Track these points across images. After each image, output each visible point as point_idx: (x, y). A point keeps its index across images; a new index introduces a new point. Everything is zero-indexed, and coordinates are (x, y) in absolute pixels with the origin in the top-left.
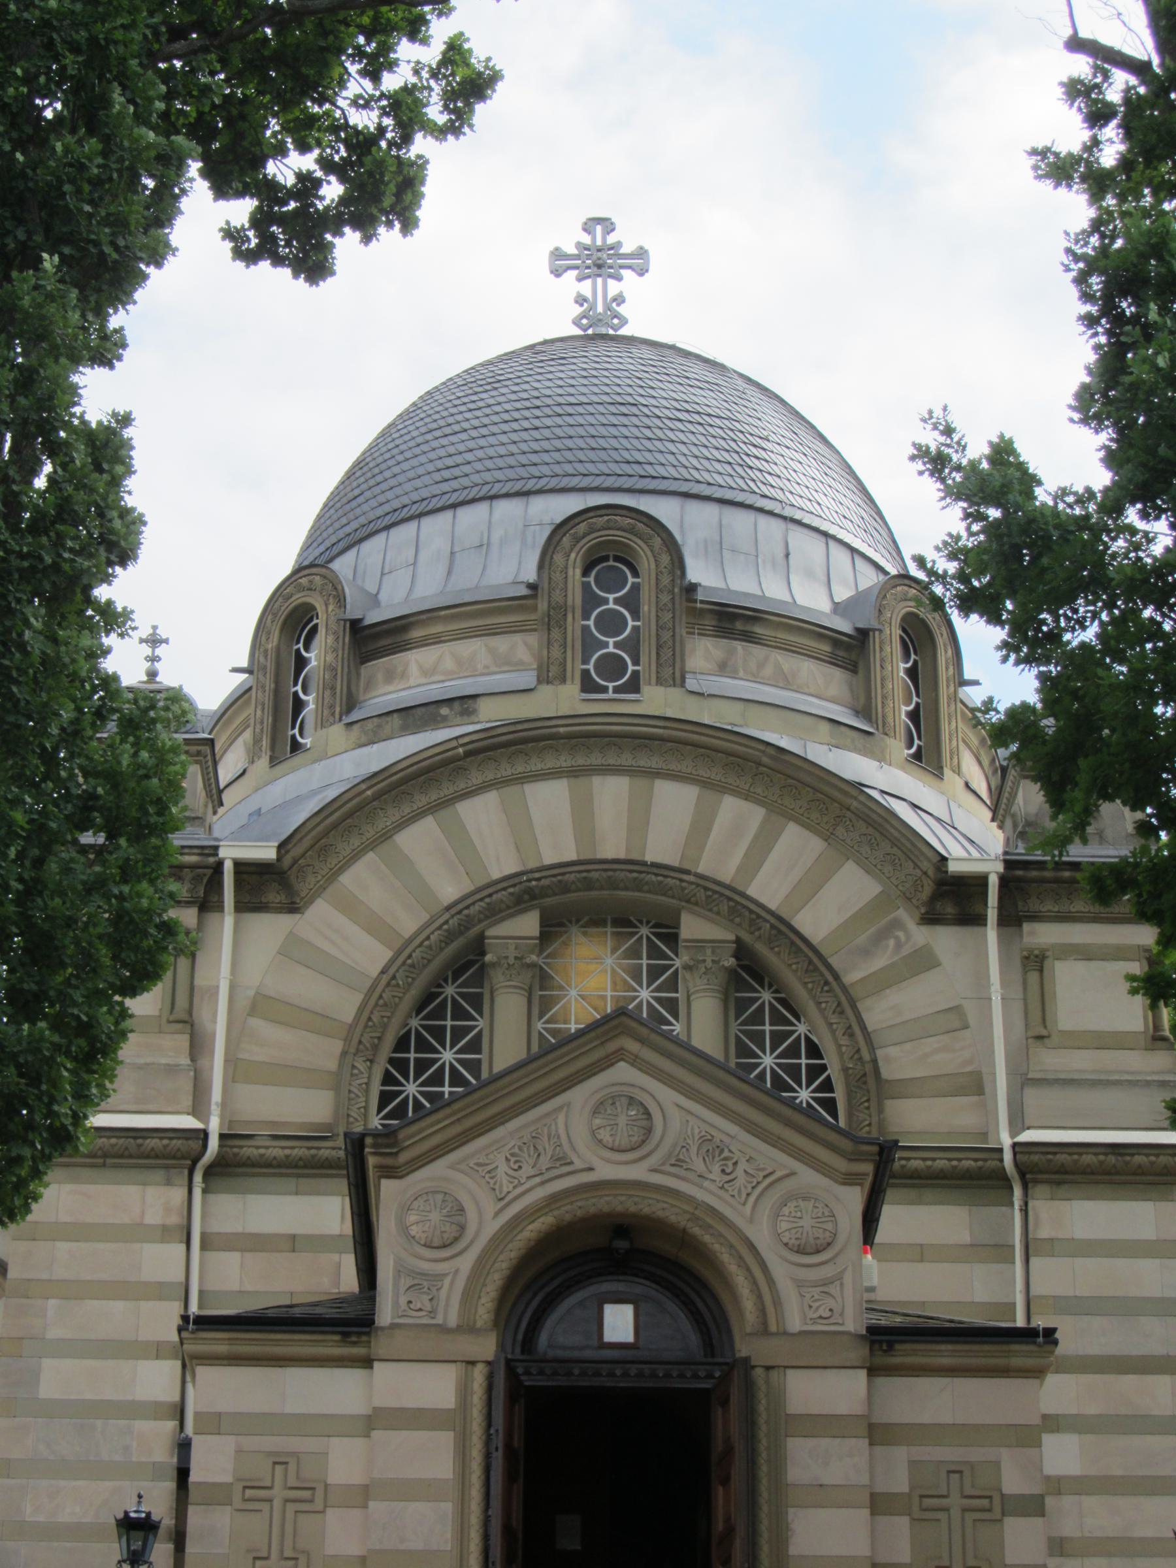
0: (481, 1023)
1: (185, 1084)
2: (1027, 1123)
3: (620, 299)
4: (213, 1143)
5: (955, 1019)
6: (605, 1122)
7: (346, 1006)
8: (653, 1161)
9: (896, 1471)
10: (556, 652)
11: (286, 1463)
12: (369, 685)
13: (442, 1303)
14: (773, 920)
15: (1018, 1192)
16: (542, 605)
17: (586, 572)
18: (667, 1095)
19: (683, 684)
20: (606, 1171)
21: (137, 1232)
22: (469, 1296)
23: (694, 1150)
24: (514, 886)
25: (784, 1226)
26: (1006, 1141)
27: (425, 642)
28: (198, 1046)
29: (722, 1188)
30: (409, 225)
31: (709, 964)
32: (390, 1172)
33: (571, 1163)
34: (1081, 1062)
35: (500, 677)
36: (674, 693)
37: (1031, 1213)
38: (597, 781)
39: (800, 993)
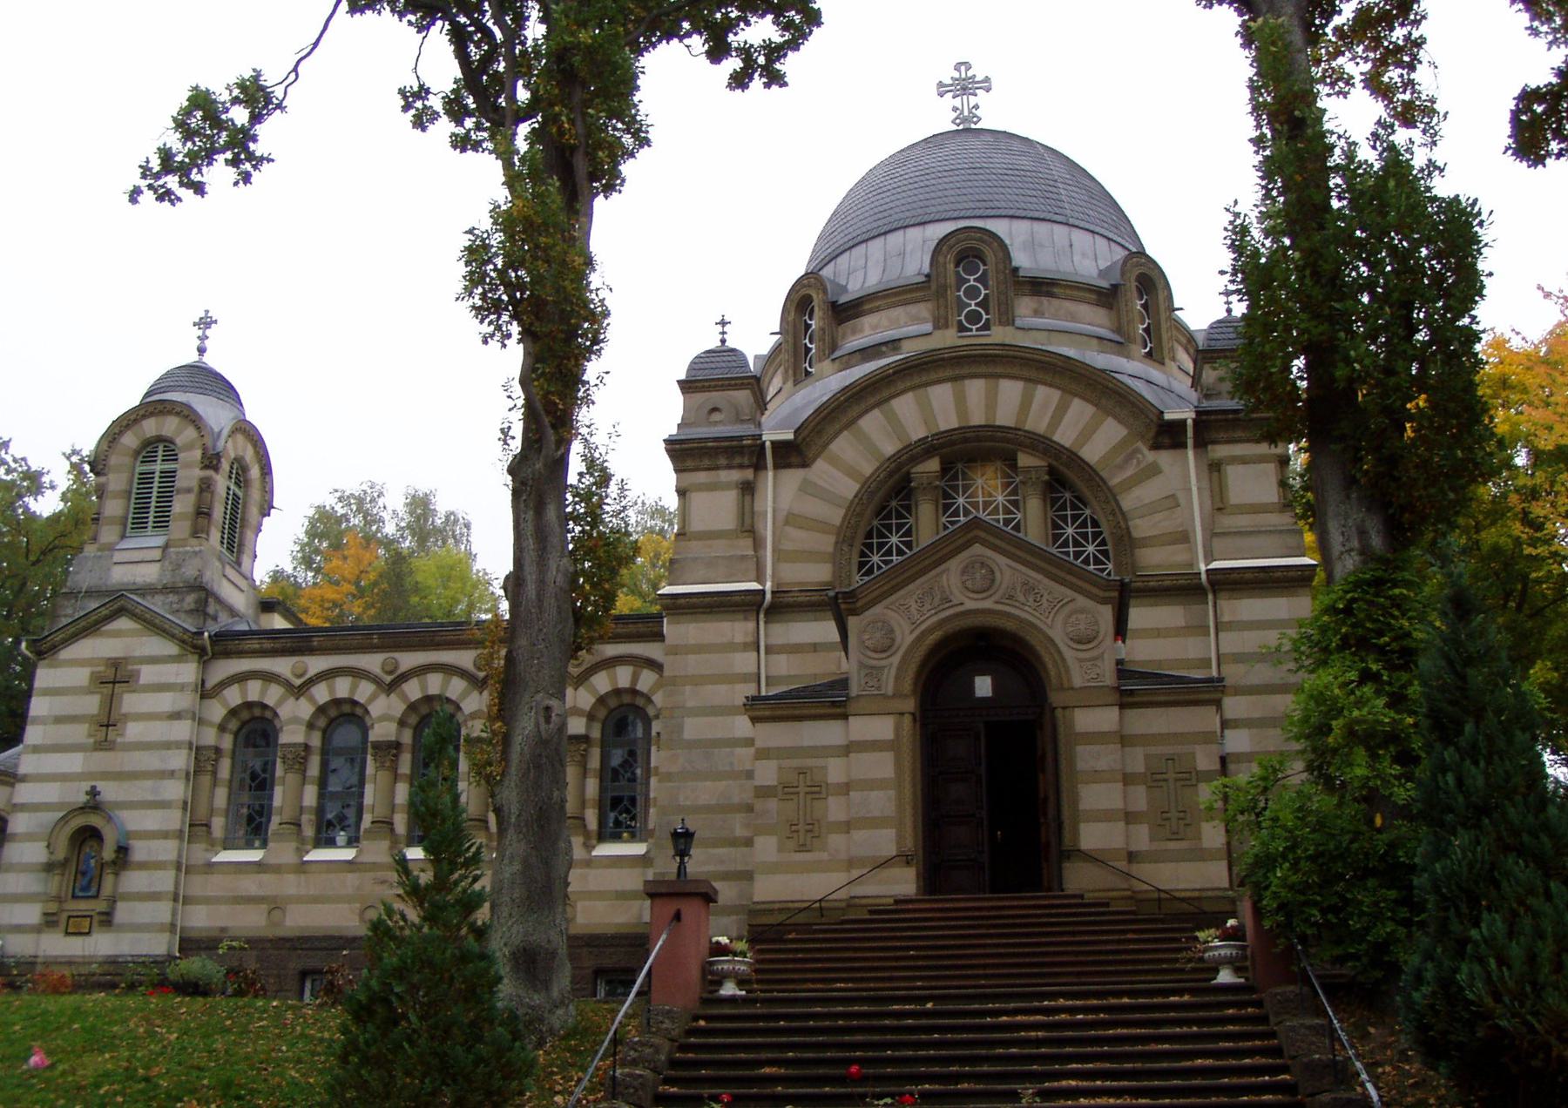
0: (911, 520)
1: (752, 565)
3: (976, 107)
4: (768, 596)
5: (1171, 502)
7: (836, 516)
8: (996, 597)
9: (1137, 761)
10: (942, 312)
12: (843, 337)
15: (1210, 597)
16: (934, 286)
17: (957, 265)
18: (1002, 560)
20: (970, 605)
21: (731, 647)
26: (1203, 568)
27: (871, 311)
28: (758, 544)
30: (679, 382)
34: (1243, 521)
35: (912, 329)
36: (1009, 329)
38: (967, 382)
39: (1087, 493)
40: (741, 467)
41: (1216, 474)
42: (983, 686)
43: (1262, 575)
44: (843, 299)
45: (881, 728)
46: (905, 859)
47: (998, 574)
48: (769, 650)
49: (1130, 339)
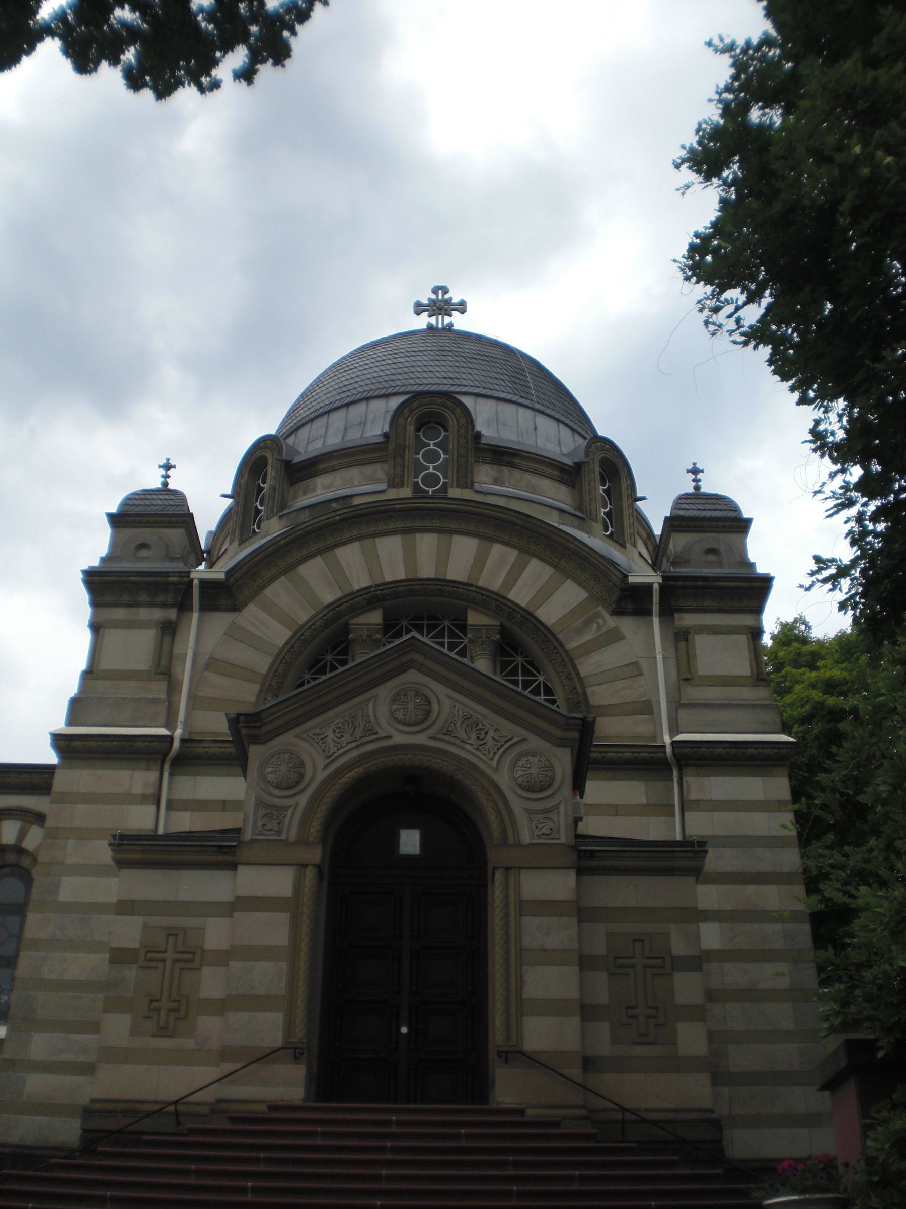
1: (162, 709)
2: (680, 730)
4: (176, 744)
5: (634, 670)
6: (399, 707)
8: (432, 732)
11: (177, 935)
13: (286, 827)
14: (523, 612)
15: (675, 773)
16: (391, 446)
17: (418, 430)
18: (441, 690)
19: (472, 485)
21: (127, 799)
22: (305, 821)
23: (459, 724)
24: (367, 594)
25: (519, 773)
26: (667, 740)
28: (173, 687)
29: (477, 749)
31: (484, 639)
32: (256, 740)
33: (377, 733)
34: (712, 694)
35: (363, 484)
37: (684, 784)
38: (418, 536)
40: (164, 605)
41: (682, 644)
42: (410, 841)
43: (734, 751)
44: (297, 460)
45: (278, 882)
46: (292, 1051)
47: (435, 708)
48: (171, 806)
49: (594, 518)
